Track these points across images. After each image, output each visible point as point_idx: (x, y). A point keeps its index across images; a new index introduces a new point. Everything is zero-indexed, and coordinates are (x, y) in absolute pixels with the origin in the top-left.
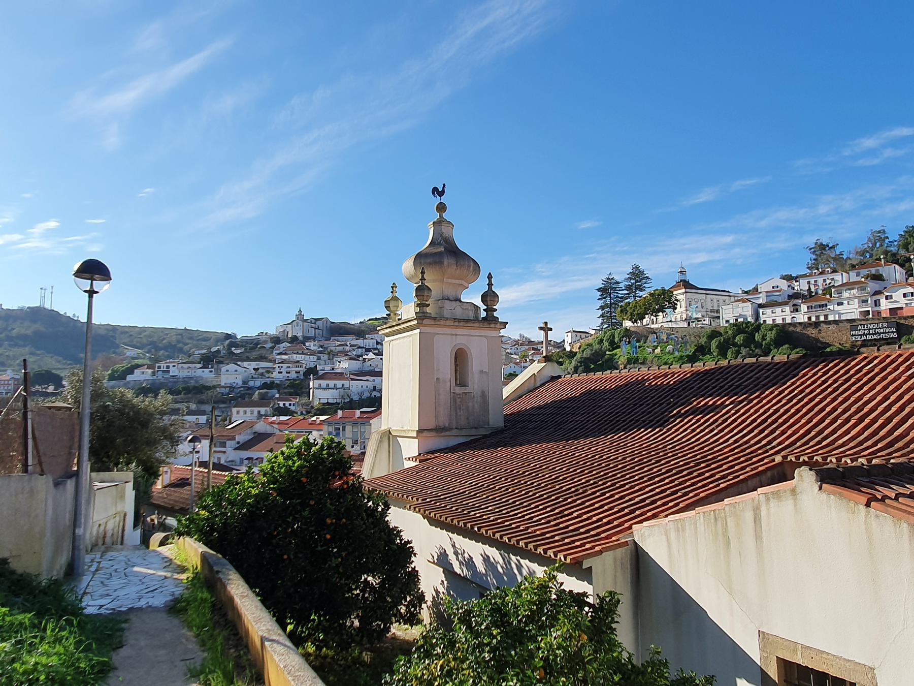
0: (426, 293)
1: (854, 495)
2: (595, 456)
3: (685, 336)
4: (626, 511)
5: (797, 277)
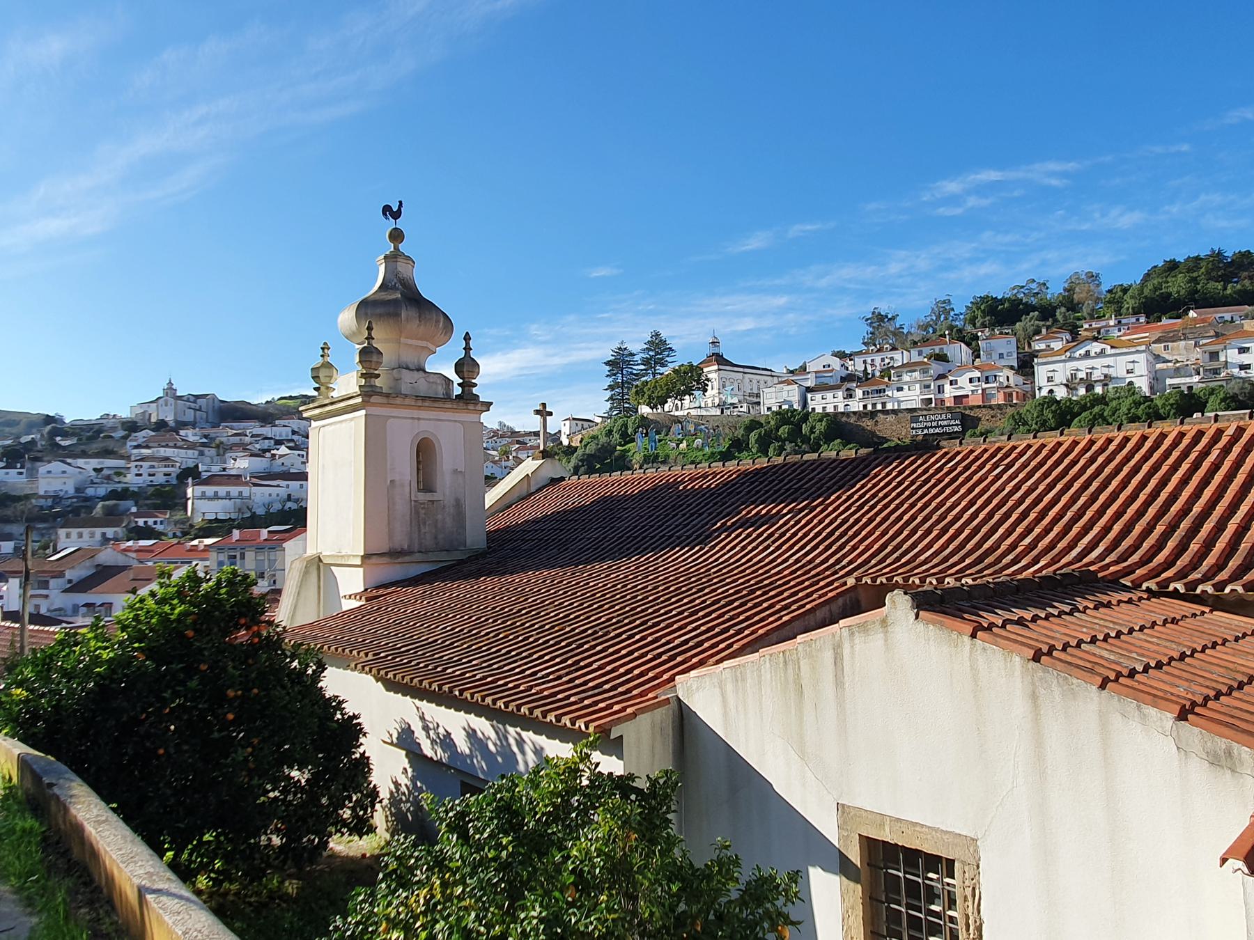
0: (375, 358)
1: (957, 623)
2: (616, 585)
3: (718, 426)
4: (664, 657)
5: (851, 355)
